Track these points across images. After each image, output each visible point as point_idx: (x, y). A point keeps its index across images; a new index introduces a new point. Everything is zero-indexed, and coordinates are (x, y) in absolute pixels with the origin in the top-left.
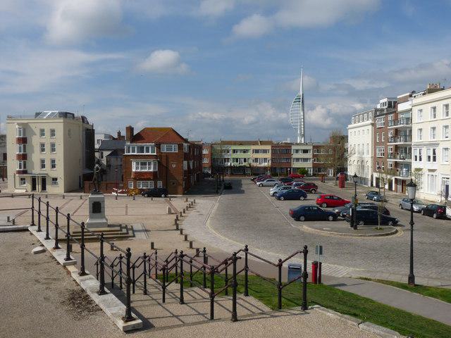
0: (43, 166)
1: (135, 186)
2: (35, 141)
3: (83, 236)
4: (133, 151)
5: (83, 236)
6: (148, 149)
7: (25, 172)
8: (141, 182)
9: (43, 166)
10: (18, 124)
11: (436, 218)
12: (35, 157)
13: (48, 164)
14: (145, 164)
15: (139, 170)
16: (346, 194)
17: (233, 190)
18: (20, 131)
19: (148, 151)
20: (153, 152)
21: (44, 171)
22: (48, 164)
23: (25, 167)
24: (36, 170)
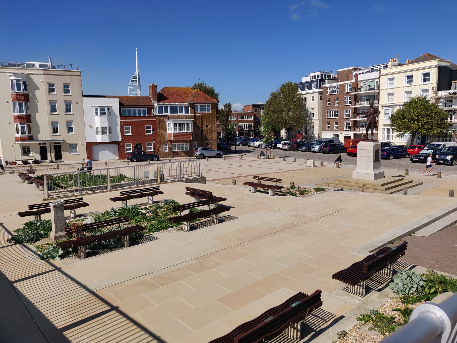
0: (55, 130)
1: (170, 148)
2: (41, 96)
3: (58, 165)
4: (181, 112)
5: (58, 165)
6: (181, 108)
7: (31, 138)
8: (176, 144)
9: (55, 130)
10: (15, 75)
11: (393, 159)
12: (43, 118)
13: (62, 128)
14: (182, 125)
15: (177, 131)
16: (322, 140)
17: (33, 115)
18: (18, 85)
19: (181, 112)
20: (187, 111)
21: (58, 137)
22: (62, 128)
23: (30, 132)
24: (45, 135)
